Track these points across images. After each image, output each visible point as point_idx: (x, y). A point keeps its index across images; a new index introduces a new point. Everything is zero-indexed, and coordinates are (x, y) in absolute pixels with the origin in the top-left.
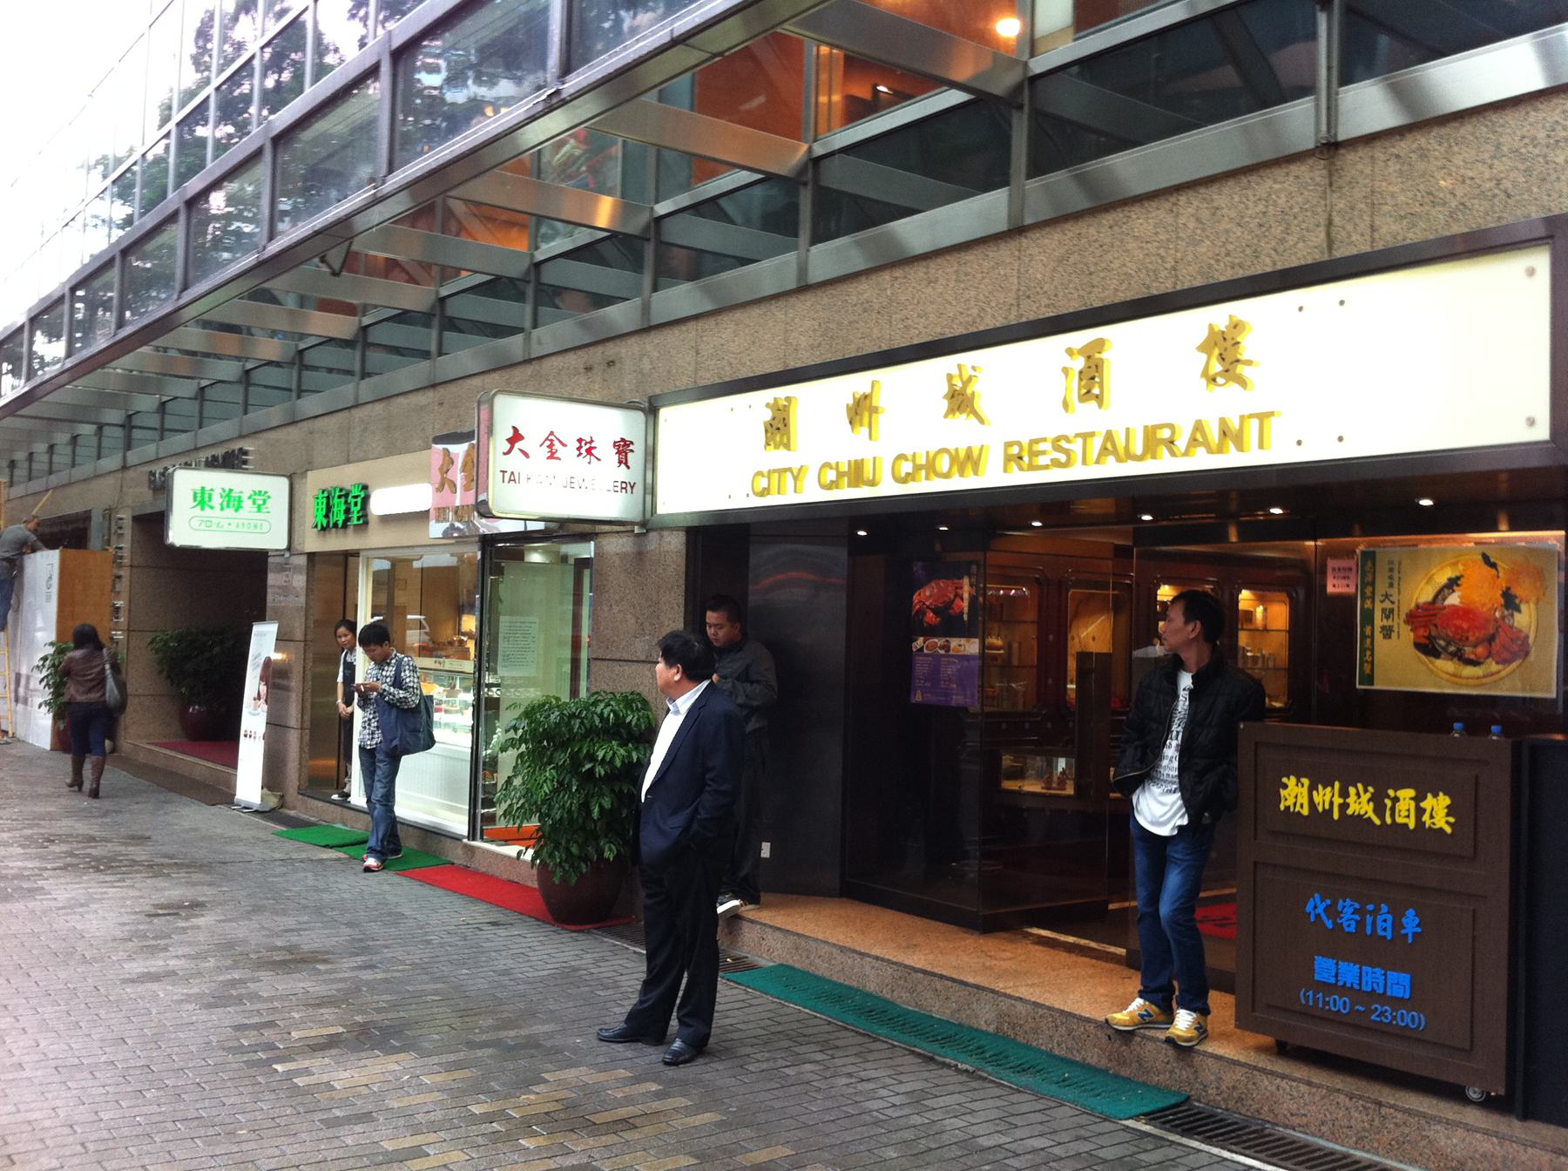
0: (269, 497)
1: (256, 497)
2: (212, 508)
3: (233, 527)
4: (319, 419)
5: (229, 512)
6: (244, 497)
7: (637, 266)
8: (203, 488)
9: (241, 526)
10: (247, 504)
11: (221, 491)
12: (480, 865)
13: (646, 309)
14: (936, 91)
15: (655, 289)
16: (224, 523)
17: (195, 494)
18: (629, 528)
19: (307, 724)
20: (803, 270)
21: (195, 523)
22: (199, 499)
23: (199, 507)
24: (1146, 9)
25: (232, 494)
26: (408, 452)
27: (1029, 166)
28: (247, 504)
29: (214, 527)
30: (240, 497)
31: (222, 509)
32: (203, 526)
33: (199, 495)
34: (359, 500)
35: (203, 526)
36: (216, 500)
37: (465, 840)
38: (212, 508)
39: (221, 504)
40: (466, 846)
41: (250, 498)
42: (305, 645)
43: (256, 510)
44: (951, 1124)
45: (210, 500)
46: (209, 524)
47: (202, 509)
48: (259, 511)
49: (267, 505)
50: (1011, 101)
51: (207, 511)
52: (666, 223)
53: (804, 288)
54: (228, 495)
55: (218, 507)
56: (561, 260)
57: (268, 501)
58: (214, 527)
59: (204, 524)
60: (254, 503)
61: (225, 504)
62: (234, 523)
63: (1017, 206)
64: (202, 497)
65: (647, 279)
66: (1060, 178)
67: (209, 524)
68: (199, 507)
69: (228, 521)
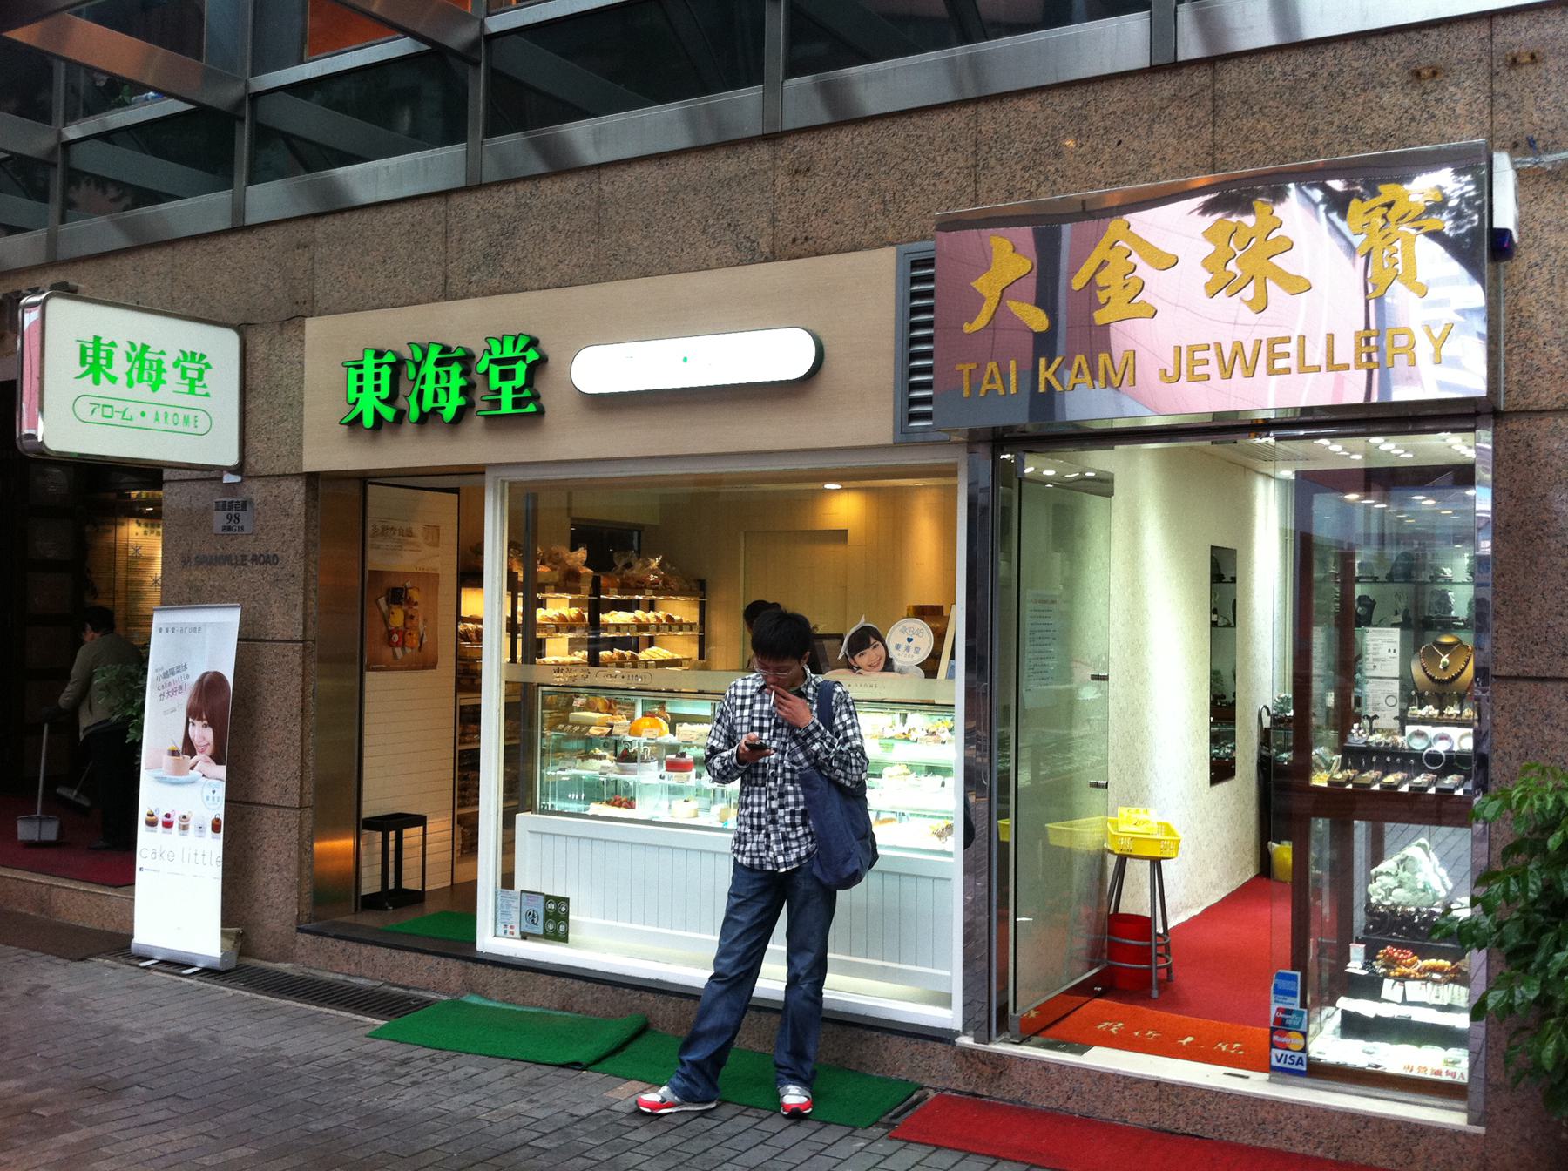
0: (208, 366)
1: (187, 365)
2: (113, 380)
3: (149, 421)
4: (385, 209)
5: (142, 391)
6: (168, 362)
7: (42, 196)
8: (97, 339)
9: (161, 418)
10: (172, 375)
11: (128, 348)
12: (1009, 1090)
13: (52, 240)
14: (387, 38)
15: (63, 220)
16: (134, 410)
17: (83, 349)
18: (213, 475)
19: (309, 798)
20: (238, 209)
21: (84, 408)
22: (90, 360)
23: (90, 376)
24: (383, 39)
25: (147, 356)
26: (672, 270)
27: (486, 128)
28: (172, 375)
29: (117, 419)
30: (160, 362)
31: (130, 385)
32: (97, 416)
33: (90, 352)
34: (520, 369)
35: (97, 416)
36: (120, 366)
37: (966, 1041)
38: (113, 380)
39: (129, 373)
40: (966, 1053)
41: (175, 365)
42: (305, 648)
43: (186, 389)
44: (552, 1141)
45: (109, 365)
46: (108, 411)
47: (96, 382)
48: (191, 392)
49: (205, 380)
50: (468, 56)
51: (105, 388)
52: (75, 149)
53: (240, 228)
54: (140, 358)
55: (122, 380)
56: (282, 93)
57: (207, 373)
58: (117, 419)
59: (98, 412)
60: (183, 377)
61: (134, 374)
62: (150, 411)
63: (472, 162)
64: (96, 357)
65: (54, 208)
66: (512, 141)
67: (108, 411)
68: (90, 376)
69: (141, 407)
